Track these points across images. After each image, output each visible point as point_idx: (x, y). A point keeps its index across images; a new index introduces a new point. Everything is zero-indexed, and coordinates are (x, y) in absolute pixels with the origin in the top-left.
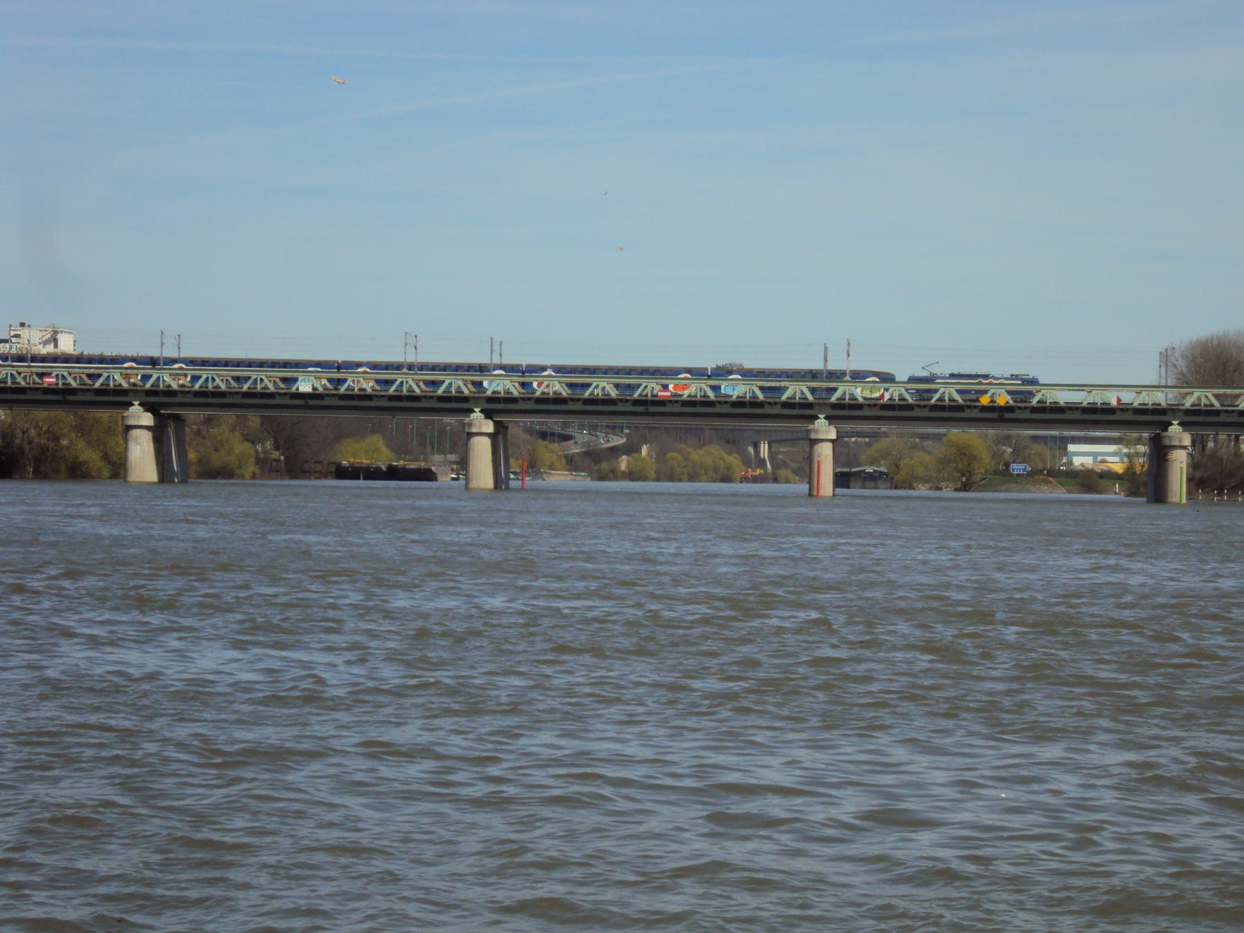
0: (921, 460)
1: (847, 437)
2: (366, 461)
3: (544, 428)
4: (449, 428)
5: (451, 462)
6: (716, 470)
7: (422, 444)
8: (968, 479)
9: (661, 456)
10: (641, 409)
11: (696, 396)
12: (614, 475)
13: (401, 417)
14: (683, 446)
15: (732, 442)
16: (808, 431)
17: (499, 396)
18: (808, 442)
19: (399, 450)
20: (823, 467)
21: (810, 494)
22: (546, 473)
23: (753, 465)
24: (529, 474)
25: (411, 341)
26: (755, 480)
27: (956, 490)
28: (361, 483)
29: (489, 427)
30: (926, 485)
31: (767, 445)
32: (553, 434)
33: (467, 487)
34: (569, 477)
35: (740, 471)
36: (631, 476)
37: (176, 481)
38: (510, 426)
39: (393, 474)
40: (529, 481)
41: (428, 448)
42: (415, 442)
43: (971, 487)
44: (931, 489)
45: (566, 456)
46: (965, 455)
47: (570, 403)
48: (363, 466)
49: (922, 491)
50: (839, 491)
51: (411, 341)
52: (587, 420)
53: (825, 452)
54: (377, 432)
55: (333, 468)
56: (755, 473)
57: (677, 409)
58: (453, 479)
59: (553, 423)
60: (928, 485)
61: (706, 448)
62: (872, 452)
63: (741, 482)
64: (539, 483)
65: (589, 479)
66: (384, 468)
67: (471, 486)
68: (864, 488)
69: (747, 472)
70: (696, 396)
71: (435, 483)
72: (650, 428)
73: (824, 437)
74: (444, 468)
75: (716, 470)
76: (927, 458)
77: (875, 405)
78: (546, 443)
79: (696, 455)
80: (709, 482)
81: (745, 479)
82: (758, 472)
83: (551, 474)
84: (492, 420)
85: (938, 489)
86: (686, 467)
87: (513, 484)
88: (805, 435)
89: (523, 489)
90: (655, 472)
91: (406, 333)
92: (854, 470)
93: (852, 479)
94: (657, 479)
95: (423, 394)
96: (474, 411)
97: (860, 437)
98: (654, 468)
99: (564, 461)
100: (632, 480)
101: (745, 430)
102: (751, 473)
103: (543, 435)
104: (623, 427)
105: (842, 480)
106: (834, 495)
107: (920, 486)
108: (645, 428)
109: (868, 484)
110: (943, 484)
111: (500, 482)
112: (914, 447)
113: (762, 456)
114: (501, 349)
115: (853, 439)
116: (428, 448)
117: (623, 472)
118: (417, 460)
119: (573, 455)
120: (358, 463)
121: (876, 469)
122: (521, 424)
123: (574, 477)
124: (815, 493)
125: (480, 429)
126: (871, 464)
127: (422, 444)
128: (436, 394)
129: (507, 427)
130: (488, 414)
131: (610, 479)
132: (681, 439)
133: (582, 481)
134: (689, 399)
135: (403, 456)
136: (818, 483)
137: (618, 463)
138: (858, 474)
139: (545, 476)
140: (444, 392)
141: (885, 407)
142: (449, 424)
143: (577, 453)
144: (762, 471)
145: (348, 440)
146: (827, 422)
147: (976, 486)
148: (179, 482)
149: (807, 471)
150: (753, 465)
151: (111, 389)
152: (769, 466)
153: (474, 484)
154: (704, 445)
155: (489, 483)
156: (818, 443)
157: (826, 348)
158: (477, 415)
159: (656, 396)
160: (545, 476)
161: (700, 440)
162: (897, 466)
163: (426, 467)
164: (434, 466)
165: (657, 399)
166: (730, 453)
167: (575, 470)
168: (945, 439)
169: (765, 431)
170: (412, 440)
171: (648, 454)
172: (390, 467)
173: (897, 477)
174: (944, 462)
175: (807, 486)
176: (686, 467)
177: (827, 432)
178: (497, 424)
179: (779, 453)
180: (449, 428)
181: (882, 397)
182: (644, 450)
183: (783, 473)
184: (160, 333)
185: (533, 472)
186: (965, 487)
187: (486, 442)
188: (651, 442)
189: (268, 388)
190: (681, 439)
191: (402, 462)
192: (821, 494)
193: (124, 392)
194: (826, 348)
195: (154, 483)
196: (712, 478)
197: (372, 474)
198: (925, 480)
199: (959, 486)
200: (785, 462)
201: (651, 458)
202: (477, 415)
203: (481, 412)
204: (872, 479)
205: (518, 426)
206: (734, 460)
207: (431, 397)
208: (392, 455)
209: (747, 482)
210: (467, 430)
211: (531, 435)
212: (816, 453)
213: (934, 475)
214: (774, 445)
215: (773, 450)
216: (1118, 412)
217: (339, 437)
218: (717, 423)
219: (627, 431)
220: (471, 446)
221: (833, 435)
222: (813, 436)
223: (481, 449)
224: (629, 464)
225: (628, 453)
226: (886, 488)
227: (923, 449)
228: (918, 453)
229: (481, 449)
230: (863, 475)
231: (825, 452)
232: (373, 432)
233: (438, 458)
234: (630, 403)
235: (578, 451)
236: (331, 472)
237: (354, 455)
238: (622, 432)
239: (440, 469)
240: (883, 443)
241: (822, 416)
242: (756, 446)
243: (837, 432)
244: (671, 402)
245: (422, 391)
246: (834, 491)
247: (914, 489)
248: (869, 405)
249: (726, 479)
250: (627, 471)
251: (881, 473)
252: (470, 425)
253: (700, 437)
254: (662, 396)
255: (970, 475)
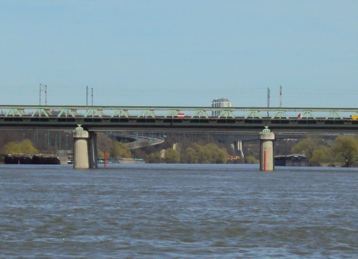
0: (323, 151)
1: (285, 138)
2: (21, 154)
3: (120, 135)
4: (67, 135)
5: (69, 154)
6: (213, 157)
7: (53, 144)
8: (349, 160)
9: (183, 149)
10: (168, 124)
11: (92, 116)
12: (158, 160)
13: (38, 130)
14: (195, 144)
15: (222, 141)
16: (259, 135)
17: (333, 120)
18: (260, 141)
19: (41, 148)
20: (267, 155)
21: (261, 170)
22: (120, 159)
23: (234, 154)
24: (109, 160)
25: (43, 88)
26: (235, 162)
27: (343, 166)
28: (19, 166)
29: (86, 134)
30: (327, 164)
31: (241, 143)
32: (124, 138)
33: (74, 168)
34: (133, 162)
35: (226, 157)
36: (167, 160)
37: (94, 167)
38: (98, 133)
39: (36, 161)
40: (110, 164)
41: (56, 146)
42: (49, 143)
43: (351, 165)
44: (329, 166)
45: (131, 151)
46: (347, 147)
47: (130, 121)
48: (20, 156)
49: (325, 167)
50: (276, 167)
51: (43, 88)
52: (143, 131)
53: (268, 147)
54: (29, 138)
55: (3, 158)
56: (235, 159)
57: (215, 124)
58: (69, 163)
59: (124, 132)
60: (328, 164)
61: (208, 145)
62: (297, 146)
63: (227, 163)
64: (116, 165)
65: (144, 162)
66: (31, 158)
67: (76, 167)
68: (293, 165)
69: (231, 158)
70: (92, 116)
71: (59, 165)
72: (177, 134)
73: (268, 139)
74: (64, 157)
75: (213, 157)
76: (326, 149)
77: (295, 121)
78: (120, 143)
79: (202, 149)
80: (210, 163)
81: (229, 162)
82: (237, 157)
83: (123, 160)
84: (88, 131)
85: (333, 166)
86: (197, 155)
87: (99, 165)
88: (257, 138)
89: (105, 168)
90: (180, 158)
91: (41, 84)
92: (288, 156)
93: (287, 161)
94: (181, 162)
95: (50, 117)
96: (265, 128)
97: (292, 138)
98: (180, 156)
99: (130, 153)
100: (167, 163)
101: (229, 135)
102: (232, 158)
103: (119, 139)
104: (162, 134)
105: (278, 162)
106: (274, 169)
107: (323, 164)
108: (175, 134)
109: (295, 164)
110: (335, 163)
111: (92, 165)
112: (321, 143)
113: (239, 149)
114: (92, 92)
115: (288, 139)
116: (56, 146)
117: (163, 159)
118: (50, 153)
119: (135, 149)
120: (17, 155)
121: (300, 155)
122: (107, 133)
123: (136, 161)
124: (263, 169)
125: (81, 136)
126: (297, 152)
127: (53, 144)
128: (57, 117)
129: (96, 135)
130: (85, 128)
131: (156, 163)
132: (194, 140)
133: (141, 164)
134: (194, 118)
135: (42, 150)
136: (265, 163)
137: (160, 154)
138: (290, 158)
139: (120, 161)
140: (61, 116)
141: (301, 122)
142: (68, 133)
143: (138, 149)
144: (239, 157)
145: (12, 143)
146: (269, 130)
147: (353, 164)
148: (95, 168)
149: (260, 157)
150: (234, 154)
151: (66, 118)
152: (242, 154)
153: (78, 166)
154: (207, 143)
155: (86, 165)
156: (77, 140)
157: (269, 91)
158: (79, 129)
159: (177, 117)
160: (120, 161)
161: (205, 141)
162: (311, 154)
163: (54, 157)
164: (58, 156)
165: (177, 118)
166: (221, 148)
167: (137, 158)
168: (337, 139)
169: (240, 135)
170: (47, 141)
171: (177, 149)
172: (35, 157)
173: (311, 160)
174: (336, 151)
175: (259, 165)
176: (197, 155)
177: (270, 135)
178: (91, 133)
179: (248, 147)
180: (67, 135)
181: (299, 116)
182: (174, 146)
183: (250, 158)
184: (86, 87)
185: (113, 159)
186: (347, 165)
187: (85, 142)
188: (178, 142)
189: (45, 116)
190: (194, 140)
191: (41, 155)
192: (267, 169)
193: (73, 120)
194: (269, 91)
195: (87, 169)
196: (211, 161)
197: (24, 161)
198: (326, 161)
199: (344, 164)
200: (251, 152)
201: (178, 151)
202: (79, 129)
203: (81, 126)
204: (298, 161)
205: (101, 133)
206: (223, 151)
207: (54, 119)
208: (36, 150)
209: (231, 163)
210: (74, 136)
211: (112, 139)
212: (264, 147)
213: (331, 158)
214: (245, 143)
215: (245, 145)
216: (318, 123)
217: (7, 140)
218: (212, 131)
219: (165, 136)
220: (76, 145)
221: (273, 137)
222: (262, 138)
223: (82, 147)
224: (166, 154)
225: (165, 148)
226: (305, 166)
227: (326, 145)
228: (322, 146)
229: (82, 147)
230: (293, 159)
231: (268, 147)
232: (26, 138)
233: (61, 152)
234: (351, 123)
235: (138, 147)
236: (2, 160)
237: (15, 150)
238: (162, 137)
239: (61, 158)
240: (302, 142)
241: (267, 127)
242: (236, 144)
243: (275, 135)
244: (184, 120)
245: (49, 116)
246: (273, 167)
247: (320, 166)
248: (292, 121)
249: (219, 162)
250: (165, 157)
251: (303, 158)
252: (75, 134)
253: (205, 139)
254: (180, 117)
255: (351, 158)
